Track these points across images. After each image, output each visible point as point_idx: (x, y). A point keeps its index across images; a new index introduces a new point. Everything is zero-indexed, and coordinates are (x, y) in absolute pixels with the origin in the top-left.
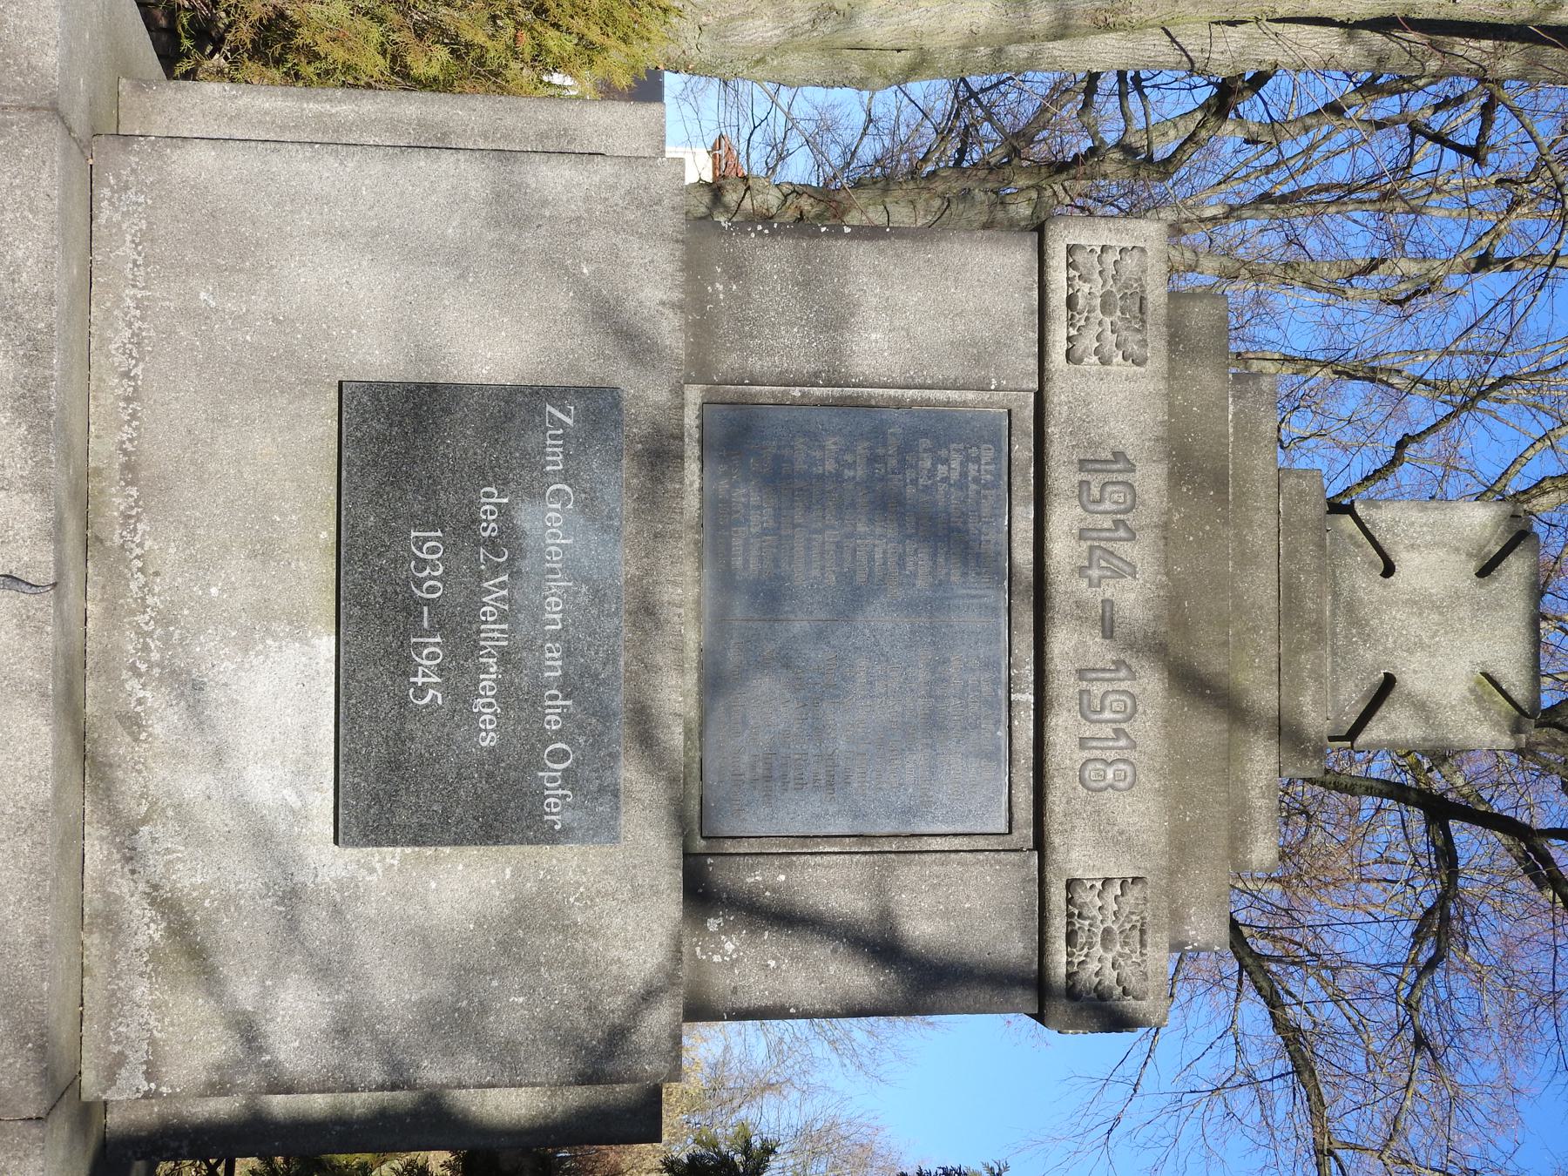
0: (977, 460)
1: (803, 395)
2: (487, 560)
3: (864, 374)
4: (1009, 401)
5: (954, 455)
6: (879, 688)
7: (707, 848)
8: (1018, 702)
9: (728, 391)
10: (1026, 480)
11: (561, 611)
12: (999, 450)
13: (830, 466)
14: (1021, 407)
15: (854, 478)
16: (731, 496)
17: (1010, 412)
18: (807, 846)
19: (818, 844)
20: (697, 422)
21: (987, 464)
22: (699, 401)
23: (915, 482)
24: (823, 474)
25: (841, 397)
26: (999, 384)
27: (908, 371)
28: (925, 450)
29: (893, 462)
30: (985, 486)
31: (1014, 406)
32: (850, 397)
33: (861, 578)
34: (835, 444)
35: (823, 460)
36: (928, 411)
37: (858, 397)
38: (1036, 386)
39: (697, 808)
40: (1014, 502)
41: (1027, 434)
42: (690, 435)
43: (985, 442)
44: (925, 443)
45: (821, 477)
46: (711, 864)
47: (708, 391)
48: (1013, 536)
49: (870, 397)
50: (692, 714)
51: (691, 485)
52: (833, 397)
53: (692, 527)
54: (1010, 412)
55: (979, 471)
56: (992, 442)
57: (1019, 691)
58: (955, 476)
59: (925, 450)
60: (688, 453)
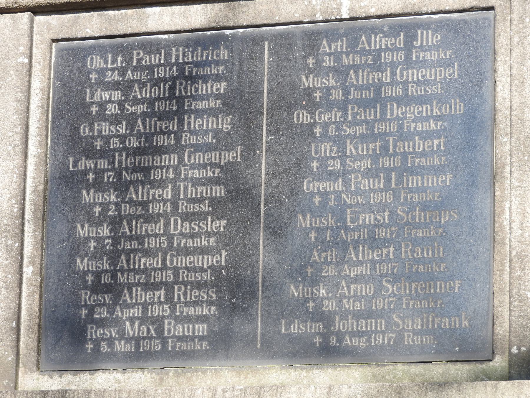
0: (102, 72)
1: (32, 263)
2: (113, 212)
3: (9, 200)
4: (42, 42)
5: (97, 98)
6: (335, 165)
7: (503, 353)
8: (351, 10)
9: (27, 344)
10: (122, 19)
11: (366, 119)
12: (92, 50)
13: (105, 231)
14: (49, 29)
15: (116, 204)
16: (133, 338)
17: (54, 41)
18: (503, 239)
19: (502, 227)
20: (56, 376)
21: (106, 62)
22: (35, 375)
23: (122, 138)
24: (112, 238)
25: (35, 223)
26: (23, 54)
27: (8, 152)
28: (92, 129)
29: (103, 164)
30: (129, 61)
31: (48, 37)
32: (35, 213)
33: (219, 191)
34: (83, 227)
35: (98, 239)
36: (53, 129)
37: (35, 204)
38: (26, 16)
39: (459, 366)
40: (143, 30)
41: (76, 21)
42: (69, 384)
43: (85, 65)
44: (84, 130)
45: (116, 241)
46: (519, 349)
47: (25, 366)
48: (179, 28)
49: (35, 191)
50: (357, 375)
51: (118, 382)
52: (34, 231)
53: (162, 379)
54: (54, 41)
55: (113, 70)
56: (85, 58)
57: (339, 9)
58: (117, 95)
59: (92, 129)
60: (87, 385)
